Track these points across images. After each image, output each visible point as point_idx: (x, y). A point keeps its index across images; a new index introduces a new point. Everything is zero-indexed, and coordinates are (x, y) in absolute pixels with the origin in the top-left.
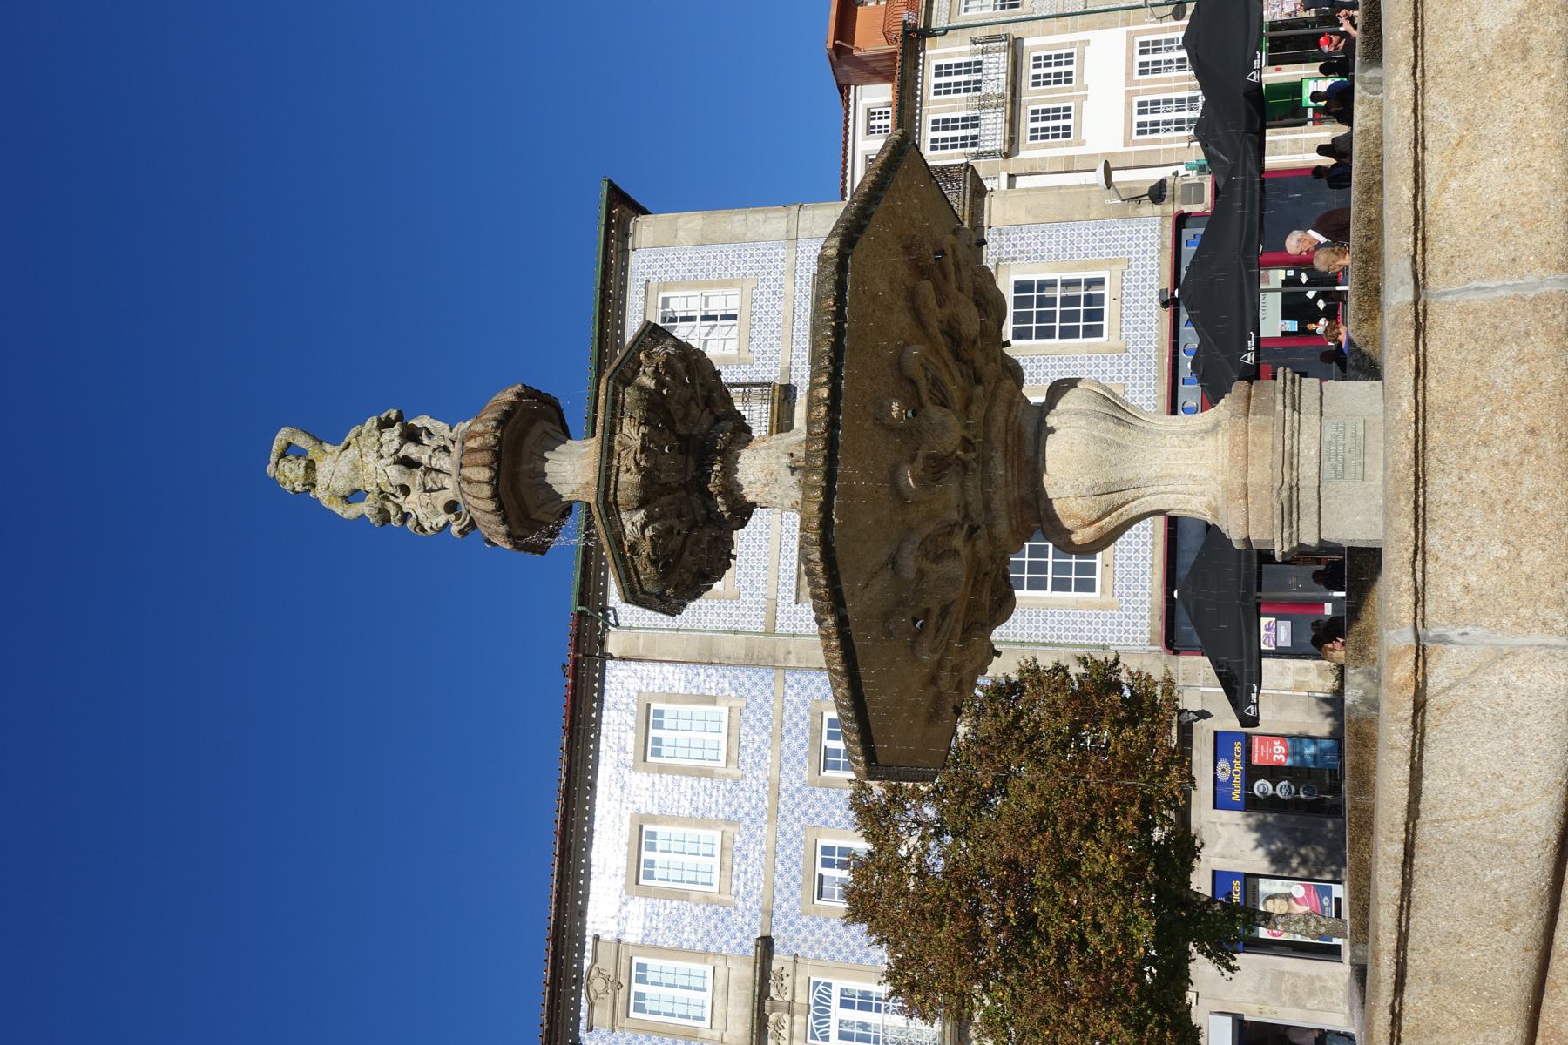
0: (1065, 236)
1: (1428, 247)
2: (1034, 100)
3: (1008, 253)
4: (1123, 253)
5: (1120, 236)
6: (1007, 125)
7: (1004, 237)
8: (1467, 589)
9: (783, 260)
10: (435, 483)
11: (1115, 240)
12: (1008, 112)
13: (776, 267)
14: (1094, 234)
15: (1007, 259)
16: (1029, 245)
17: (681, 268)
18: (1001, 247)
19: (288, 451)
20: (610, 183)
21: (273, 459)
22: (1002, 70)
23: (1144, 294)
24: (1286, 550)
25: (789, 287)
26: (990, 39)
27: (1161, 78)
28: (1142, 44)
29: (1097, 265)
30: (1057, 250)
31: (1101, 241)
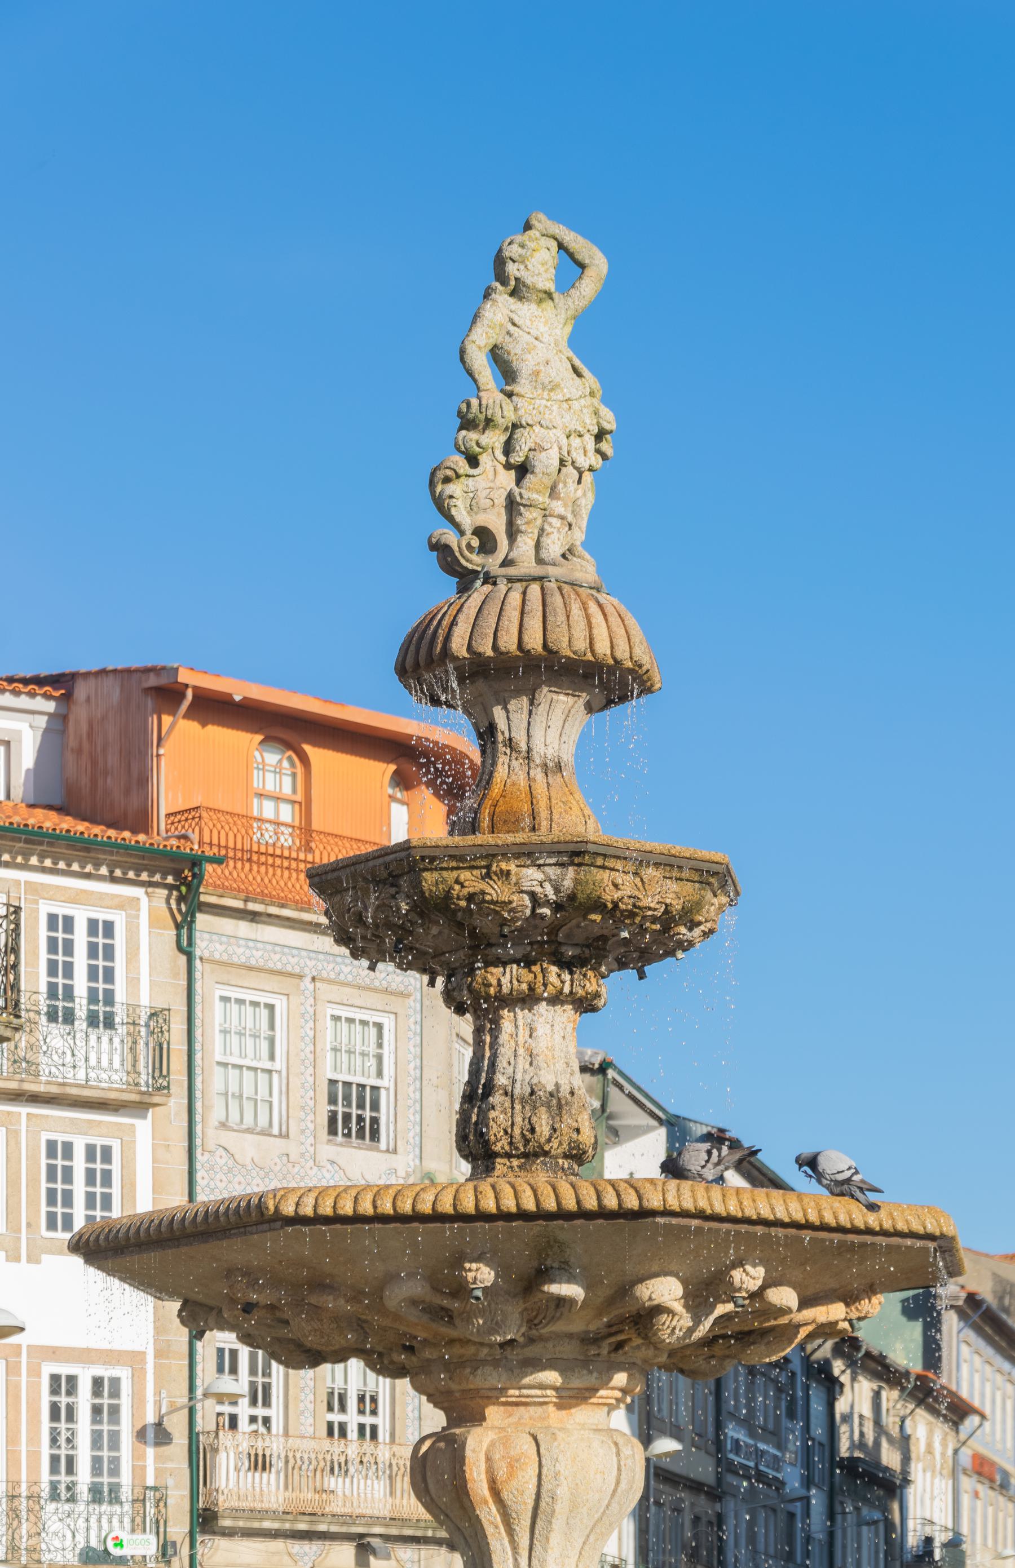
2: (18, 1143)
10: (527, 523)
22: (92, 1075)
26: (161, 1052)
27: (39, 1422)
28: (115, 1382)
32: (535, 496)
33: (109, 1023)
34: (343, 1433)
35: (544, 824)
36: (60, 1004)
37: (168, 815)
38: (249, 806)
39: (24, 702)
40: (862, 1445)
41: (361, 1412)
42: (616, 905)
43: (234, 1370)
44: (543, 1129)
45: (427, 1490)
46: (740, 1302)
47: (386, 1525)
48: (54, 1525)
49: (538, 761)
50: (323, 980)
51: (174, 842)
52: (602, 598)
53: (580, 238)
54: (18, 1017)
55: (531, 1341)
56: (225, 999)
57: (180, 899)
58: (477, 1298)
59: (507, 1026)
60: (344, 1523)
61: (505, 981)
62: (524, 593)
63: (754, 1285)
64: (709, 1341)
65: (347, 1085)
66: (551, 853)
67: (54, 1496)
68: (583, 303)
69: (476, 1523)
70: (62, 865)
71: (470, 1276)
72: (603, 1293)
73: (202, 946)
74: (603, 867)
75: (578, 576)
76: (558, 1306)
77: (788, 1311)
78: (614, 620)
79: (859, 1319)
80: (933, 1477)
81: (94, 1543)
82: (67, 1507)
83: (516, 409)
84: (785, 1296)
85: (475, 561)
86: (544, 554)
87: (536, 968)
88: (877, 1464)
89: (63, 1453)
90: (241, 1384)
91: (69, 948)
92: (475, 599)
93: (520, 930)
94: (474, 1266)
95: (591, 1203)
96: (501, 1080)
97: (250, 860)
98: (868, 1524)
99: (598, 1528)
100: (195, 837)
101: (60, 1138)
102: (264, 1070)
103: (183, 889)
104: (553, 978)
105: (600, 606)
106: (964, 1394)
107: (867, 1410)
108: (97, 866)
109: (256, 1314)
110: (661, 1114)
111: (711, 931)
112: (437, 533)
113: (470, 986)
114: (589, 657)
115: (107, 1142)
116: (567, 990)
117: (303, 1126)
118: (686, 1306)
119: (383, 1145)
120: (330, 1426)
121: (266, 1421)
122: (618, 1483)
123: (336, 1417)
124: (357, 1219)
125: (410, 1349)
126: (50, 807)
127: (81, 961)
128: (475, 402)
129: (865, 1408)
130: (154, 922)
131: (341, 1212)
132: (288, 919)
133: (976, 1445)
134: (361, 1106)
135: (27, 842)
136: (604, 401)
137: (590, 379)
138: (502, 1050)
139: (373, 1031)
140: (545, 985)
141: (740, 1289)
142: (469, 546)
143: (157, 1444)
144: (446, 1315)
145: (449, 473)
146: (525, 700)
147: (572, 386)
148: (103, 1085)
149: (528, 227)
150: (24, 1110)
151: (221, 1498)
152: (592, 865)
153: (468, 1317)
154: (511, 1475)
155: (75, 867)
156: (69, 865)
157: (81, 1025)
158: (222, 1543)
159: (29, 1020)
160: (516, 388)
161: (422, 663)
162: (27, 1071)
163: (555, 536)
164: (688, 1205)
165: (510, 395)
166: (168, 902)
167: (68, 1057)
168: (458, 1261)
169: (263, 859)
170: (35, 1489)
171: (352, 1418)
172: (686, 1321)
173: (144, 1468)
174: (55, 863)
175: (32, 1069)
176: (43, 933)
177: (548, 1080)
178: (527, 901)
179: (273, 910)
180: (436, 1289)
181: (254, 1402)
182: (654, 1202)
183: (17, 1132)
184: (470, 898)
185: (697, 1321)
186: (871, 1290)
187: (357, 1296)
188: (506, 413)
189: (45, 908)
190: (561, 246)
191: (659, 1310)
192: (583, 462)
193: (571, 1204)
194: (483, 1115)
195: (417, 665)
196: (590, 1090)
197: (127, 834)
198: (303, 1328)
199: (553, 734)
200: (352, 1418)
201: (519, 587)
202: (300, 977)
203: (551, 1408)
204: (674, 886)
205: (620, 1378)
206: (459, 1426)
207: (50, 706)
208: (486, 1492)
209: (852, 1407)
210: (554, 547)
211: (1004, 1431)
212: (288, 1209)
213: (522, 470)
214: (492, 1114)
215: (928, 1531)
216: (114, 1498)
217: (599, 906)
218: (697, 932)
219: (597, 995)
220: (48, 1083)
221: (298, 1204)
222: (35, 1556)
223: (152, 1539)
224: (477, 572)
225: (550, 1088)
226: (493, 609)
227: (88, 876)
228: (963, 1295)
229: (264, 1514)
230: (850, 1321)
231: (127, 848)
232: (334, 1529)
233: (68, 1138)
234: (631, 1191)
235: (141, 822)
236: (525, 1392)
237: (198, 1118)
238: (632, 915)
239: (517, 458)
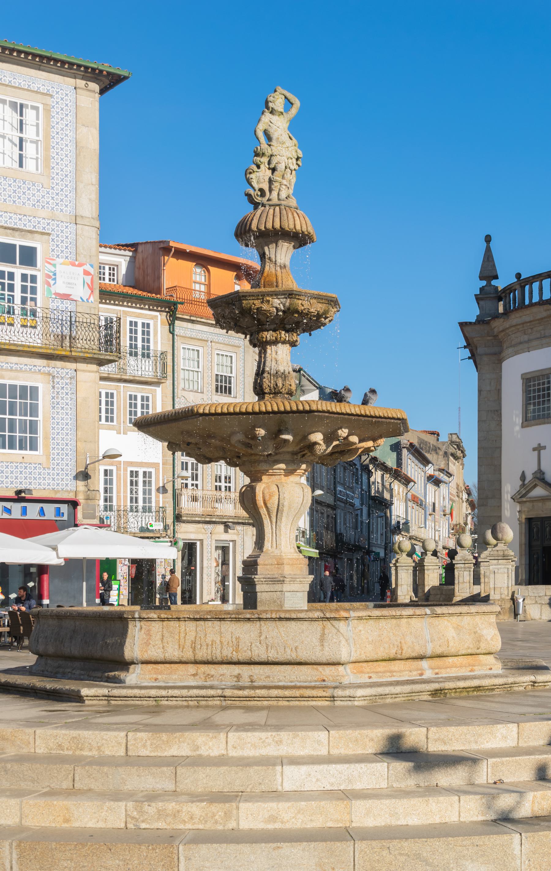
0: (67, 424)
1: (434, 618)
2: (120, 395)
3: (58, 383)
4: (53, 464)
5: (64, 462)
6: (106, 375)
7: (69, 381)
8: (360, 631)
9: (62, 210)
11: (62, 459)
12: (115, 376)
13: (57, 204)
14: (67, 445)
15: (53, 382)
16: (62, 399)
17: (60, 126)
18: (62, 378)
19: (289, 103)
20: (125, 78)
21: (285, 92)
22: (143, 373)
23: (26, 478)
24: (255, 580)
25: (43, 213)
26: (164, 365)
27: (127, 486)
28: (150, 473)
29: (46, 446)
30: (58, 419)
31: (63, 449)
32: (277, 178)
33: (148, 357)
34: (220, 489)
35: (280, 285)
36: (133, 350)
37: (167, 289)
38: (191, 286)
39: (122, 252)
40: (378, 492)
41: (226, 482)
42: (302, 312)
43: (187, 469)
44: (280, 384)
45: (244, 504)
46: (341, 441)
47: (233, 519)
48: (131, 520)
49: (278, 265)
50: (214, 342)
51: (168, 297)
52: (298, 211)
53: (291, 95)
54: (120, 354)
55: (276, 454)
56: (184, 348)
57: (170, 316)
58: (259, 440)
59: (269, 351)
60: (220, 518)
61: (268, 336)
62: (274, 210)
63: (345, 435)
64: (332, 454)
65: (222, 376)
66: (282, 294)
67: (132, 510)
68: (292, 116)
69: (259, 514)
70: (134, 305)
71: (257, 432)
72: (299, 438)
73: (177, 331)
74: (299, 299)
75: (291, 204)
76: (284, 442)
77: (355, 444)
78: (302, 218)
79: (377, 446)
80: (400, 502)
81: (144, 525)
82: (135, 514)
83: (272, 150)
84: (354, 439)
85: (259, 199)
86: (280, 197)
87: (278, 332)
88: (383, 497)
89: (134, 496)
90: (189, 474)
91: (136, 332)
92: (259, 212)
93: (273, 320)
94: (258, 429)
95: (295, 408)
96: (267, 369)
97: (191, 303)
98: (380, 517)
99: (297, 516)
100: (175, 296)
101: (133, 394)
102: (196, 371)
103: (171, 313)
104: (283, 335)
105: (298, 214)
106: (409, 475)
107: (380, 481)
108: (145, 305)
109: (191, 446)
110: (317, 385)
111: (332, 320)
112: (247, 190)
113: (257, 338)
114: (294, 230)
115: (147, 395)
116: (287, 339)
117: (208, 389)
118: (324, 442)
119: (232, 396)
120: (216, 486)
121: (197, 485)
122: (303, 500)
123: (218, 484)
124: (222, 414)
125: (239, 457)
126: (130, 286)
127: (140, 336)
128: (259, 148)
129: (379, 480)
130: (162, 324)
131: (217, 412)
132: (203, 322)
133: (413, 492)
134: (226, 383)
135: (123, 297)
136: (299, 148)
137: (294, 140)
138: (267, 359)
139: (229, 358)
140: (280, 338)
141: (340, 437)
142: (257, 195)
143: (163, 493)
144: (249, 446)
145: (251, 171)
146: (274, 245)
147: (289, 143)
148: (147, 376)
149: (275, 91)
150: (122, 385)
151: (183, 510)
152: (295, 298)
153: (257, 446)
154: (270, 498)
155: (138, 306)
156: (136, 305)
157: (140, 357)
158: (183, 525)
159: (124, 356)
160: (272, 143)
161: (243, 232)
162: (123, 372)
163: (284, 191)
164: (325, 409)
165: (270, 145)
166: (166, 317)
167: (136, 368)
168: (254, 427)
169: (196, 303)
170: (126, 508)
171: (223, 484)
172: (324, 447)
173: (159, 501)
174: (132, 304)
175: (125, 371)
176: (128, 327)
177: (281, 369)
178: (275, 310)
179: (199, 319)
180: (247, 437)
181: (193, 480)
182: (314, 408)
183: (120, 392)
184: (258, 309)
185: (328, 447)
186: (381, 437)
187: (222, 439)
188: (268, 151)
189: (129, 319)
190: (286, 98)
191: (316, 443)
192: (292, 167)
193: (288, 409)
194: (261, 380)
195: (241, 233)
196: (296, 378)
197: (154, 295)
198: (205, 450)
199: (283, 256)
200: (223, 484)
201: (272, 208)
202: (207, 341)
203: (282, 476)
204: (320, 305)
205: (304, 466)
206: (254, 482)
207: (130, 254)
208: (262, 504)
209: (375, 479)
210: (283, 195)
211: (421, 487)
212: (201, 411)
213: (274, 170)
214: (264, 380)
215: (398, 519)
216: (150, 511)
217: (297, 311)
218: (327, 320)
219: (297, 341)
220: (130, 376)
221: (204, 409)
222: (126, 530)
223: (162, 524)
224: (259, 203)
225: (282, 371)
226: (265, 215)
227: (142, 309)
228: (409, 443)
229: (196, 515)
230: (374, 447)
231: (154, 299)
232: (217, 520)
233: (135, 394)
234: (307, 404)
235: (158, 291)
236: (275, 471)
237: (176, 387)
238: (307, 314)
239: (272, 166)
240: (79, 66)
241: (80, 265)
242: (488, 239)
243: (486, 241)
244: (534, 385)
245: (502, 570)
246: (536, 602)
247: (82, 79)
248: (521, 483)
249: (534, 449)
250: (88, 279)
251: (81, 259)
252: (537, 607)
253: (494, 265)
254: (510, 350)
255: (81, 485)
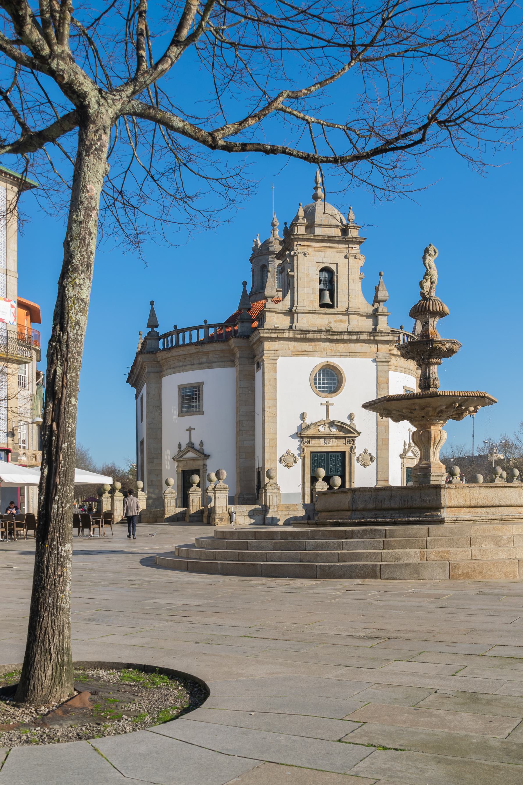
96: (431, 376)
240: (10, 175)
241: (9, 301)
242: (152, 303)
243: (151, 304)
244: (186, 392)
245: (223, 497)
246: (241, 515)
247: (10, 184)
248: (178, 449)
249: (187, 430)
250: (13, 310)
251: (9, 298)
252: (242, 517)
253: (156, 319)
254: (170, 371)
255: (10, 439)
